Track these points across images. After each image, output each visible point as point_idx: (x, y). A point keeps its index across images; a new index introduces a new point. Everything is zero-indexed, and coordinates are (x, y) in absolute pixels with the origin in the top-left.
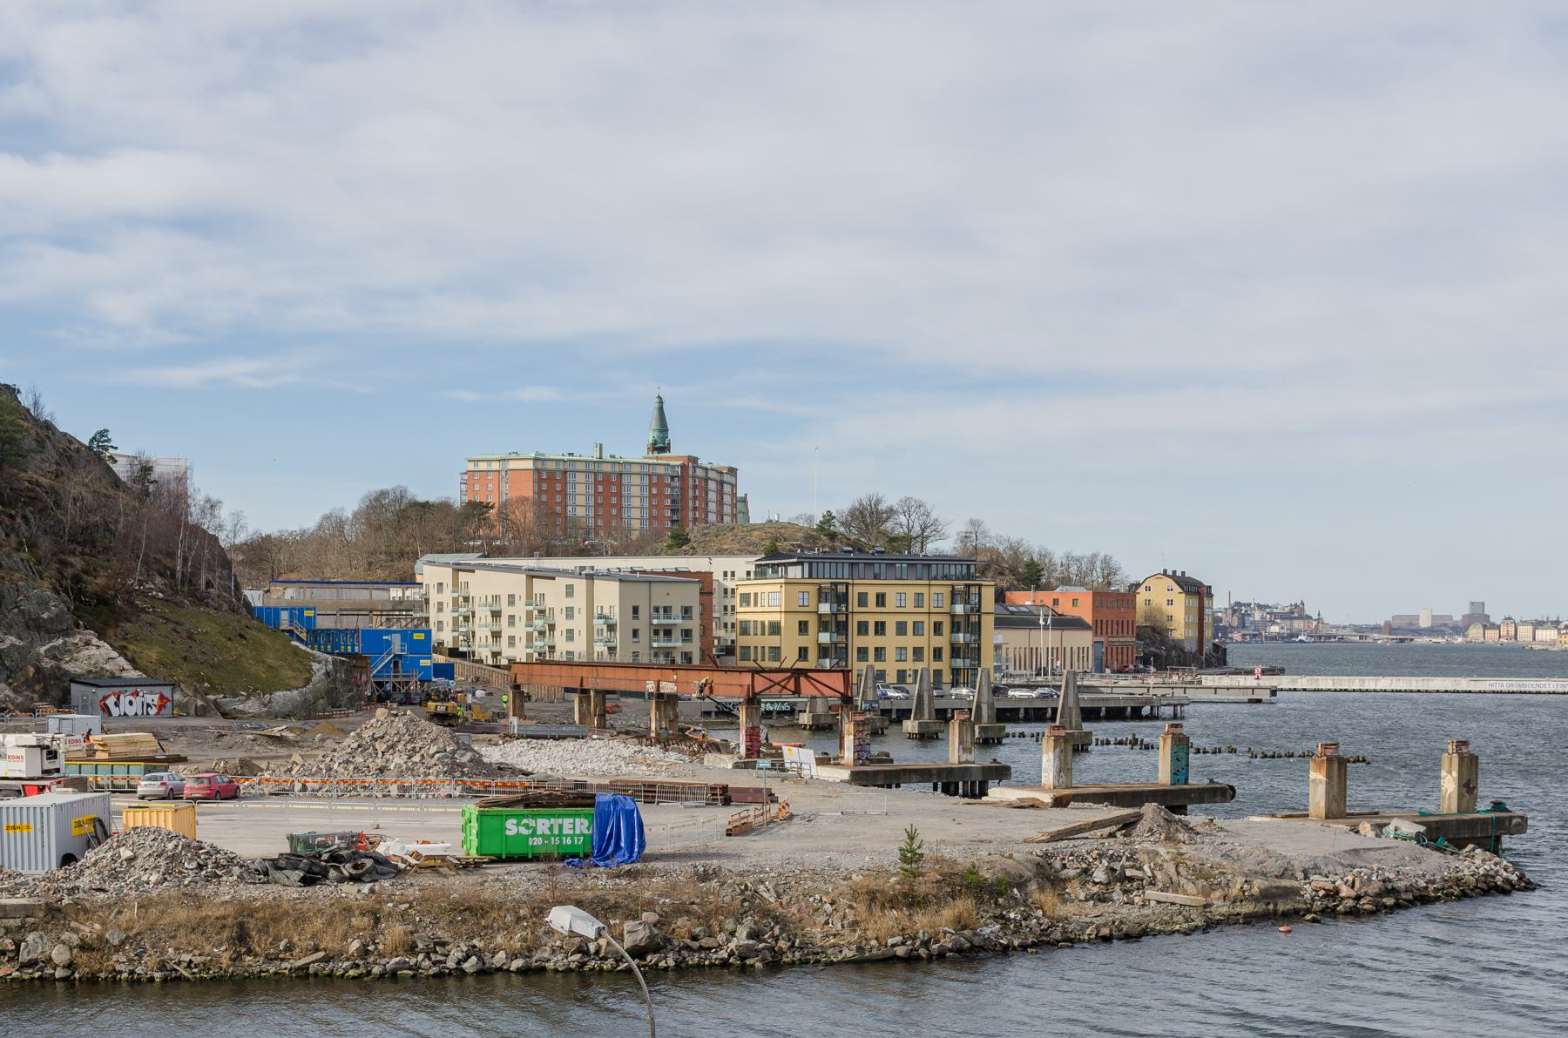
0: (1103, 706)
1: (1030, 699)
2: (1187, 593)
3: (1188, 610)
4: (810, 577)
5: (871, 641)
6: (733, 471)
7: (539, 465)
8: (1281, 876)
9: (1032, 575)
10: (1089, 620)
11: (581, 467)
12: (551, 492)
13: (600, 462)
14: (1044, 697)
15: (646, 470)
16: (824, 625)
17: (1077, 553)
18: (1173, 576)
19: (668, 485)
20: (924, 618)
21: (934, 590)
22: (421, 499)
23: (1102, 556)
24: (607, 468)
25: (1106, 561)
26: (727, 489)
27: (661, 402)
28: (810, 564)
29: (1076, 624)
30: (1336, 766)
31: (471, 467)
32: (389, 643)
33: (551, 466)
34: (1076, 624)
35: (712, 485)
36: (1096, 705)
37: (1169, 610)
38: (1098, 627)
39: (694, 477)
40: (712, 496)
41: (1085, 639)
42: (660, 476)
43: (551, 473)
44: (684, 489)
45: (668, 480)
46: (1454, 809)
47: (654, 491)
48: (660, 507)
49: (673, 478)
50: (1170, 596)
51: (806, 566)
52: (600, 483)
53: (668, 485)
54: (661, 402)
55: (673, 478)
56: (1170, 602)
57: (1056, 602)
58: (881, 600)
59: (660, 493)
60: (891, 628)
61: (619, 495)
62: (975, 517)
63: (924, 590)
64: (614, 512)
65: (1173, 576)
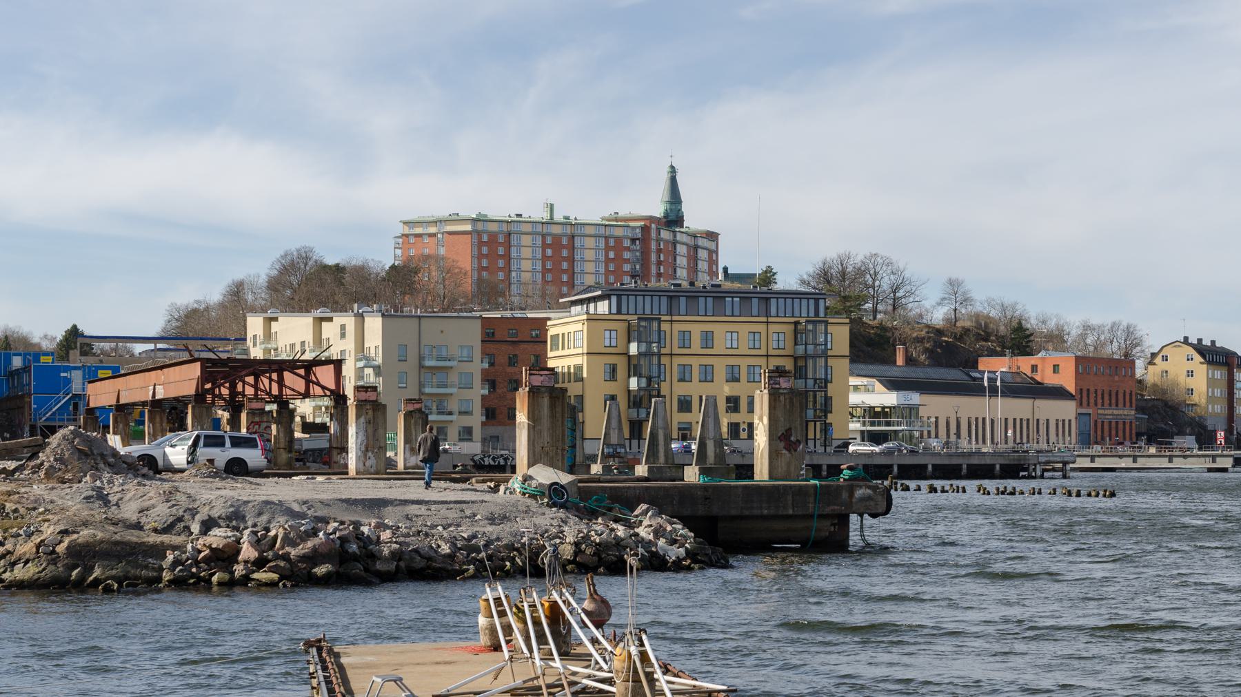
0: (964, 462)
1: (871, 455)
2: (1210, 363)
3: (1211, 382)
4: (619, 312)
5: (694, 389)
6: (712, 236)
7: (480, 226)
8: (167, 530)
9: (1020, 340)
10: (1071, 388)
11: (528, 228)
12: (492, 256)
13: (551, 222)
14: (889, 452)
15: (602, 231)
16: (634, 368)
17: (1095, 321)
18: (1200, 349)
19: (628, 249)
20: (762, 361)
21: (773, 328)
22: (330, 261)
23: (1125, 324)
24: (557, 230)
25: (1129, 331)
26: (703, 254)
27: (673, 170)
28: (619, 297)
29: (1058, 393)
30: (545, 401)
31: (407, 231)
32: (68, 381)
33: (493, 227)
34: (1058, 393)
35: (681, 249)
36: (955, 461)
37: (1191, 383)
38: (1081, 396)
39: (658, 240)
40: (682, 261)
41: (1067, 410)
42: (618, 240)
43: (493, 236)
44: (645, 253)
45: (627, 243)
46: (766, 477)
47: (612, 255)
48: (618, 273)
49: (633, 240)
50: (1190, 366)
51: (614, 299)
52: (549, 246)
53: (628, 249)
54: (673, 170)
55: (633, 240)
56: (1190, 373)
57: (1034, 368)
58: (707, 339)
59: (618, 257)
60: (720, 373)
61: (571, 260)
62: (954, 276)
63: (761, 328)
64: (501, 263)
65: (1200, 349)
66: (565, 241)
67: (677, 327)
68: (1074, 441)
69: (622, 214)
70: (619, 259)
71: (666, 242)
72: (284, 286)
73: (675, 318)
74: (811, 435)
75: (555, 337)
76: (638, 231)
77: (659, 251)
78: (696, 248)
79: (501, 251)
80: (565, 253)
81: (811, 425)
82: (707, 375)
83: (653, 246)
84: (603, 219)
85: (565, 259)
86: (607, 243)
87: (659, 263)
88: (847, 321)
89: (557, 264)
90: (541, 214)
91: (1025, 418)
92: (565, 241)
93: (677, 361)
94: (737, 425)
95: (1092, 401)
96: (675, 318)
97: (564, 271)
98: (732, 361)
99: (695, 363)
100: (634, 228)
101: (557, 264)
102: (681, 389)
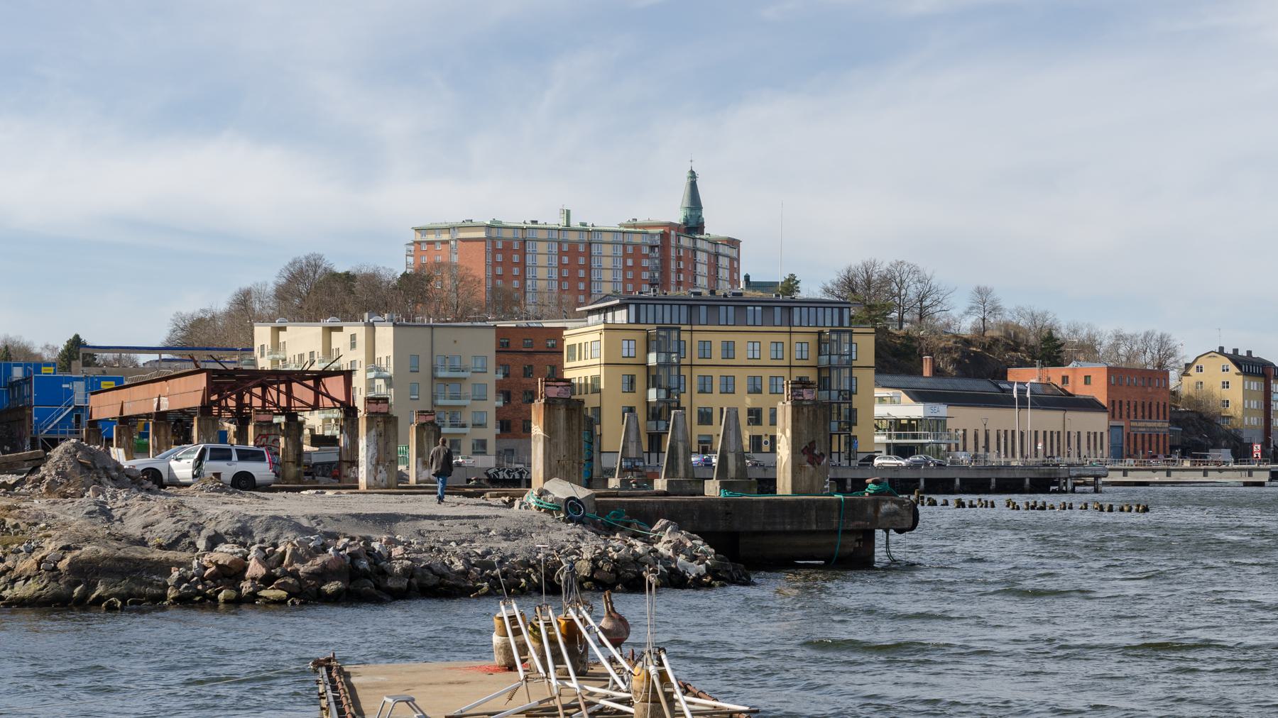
0: (993, 476)
1: (897, 468)
2: (1246, 374)
3: (1247, 394)
4: (638, 321)
5: (715, 401)
6: (734, 243)
7: (494, 233)
9: (1050, 350)
10: (1103, 400)
11: (544, 235)
12: (507, 264)
13: (568, 228)
14: (916, 466)
15: (620, 238)
16: (653, 379)
17: (1128, 331)
18: (1236, 359)
19: (647, 256)
20: (785, 372)
21: (796, 338)
22: (340, 268)
23: (1158, 334)
24: (573, 237)
25: (1163, 341)
26: (724, 262)
27: (693, 175)
28: (638, 306)
29: (1089, 405)
30: (562, 413)
31: (419, 238)
32: (70, 393)
33: (508, 234)
34: (1089, 405)
35: (702, 257)
36: (983, 475)
37: (1226, 394)
38: (1114, 408)
39: (678, 247)
40: (702, 269)
41: (1098, 422)
42: (637, 247)
43: (508, 243)
44: (665, 261)
45: (646, 250)
46: (789, 491)
47: (630, 262)
48: (637, 281)
49: (652, 248)
50: (1225, 377)
51: (632, 308)
52: (566, 253)
53: (647, 256)
54: (693, 175)
55: (652, 248)
56: (1226, 385)
57: (1065, 379)
58: (729, 349)
59: (637, 265)
60: (742, 384)
61: (588, 268)
62: (982, 285)
63: (784, 338)
64: (516, 271)
65: (1236, 359)
66: (581, 248)
67: (698, 337)
68: (1106, 454)
69: (640, 220)
70: (637, 267)
71: (686, 249)
72: (292, 295)
73: (695, 328)
74: (835, 448)
75: (572, 347)
76: (657, 238)
77: (679, 259)
78: (717, 255)
79: (516, 258)
80: (582, 261)
81: (835, 438)
82: (728, 387)
83: (673, 253)
84: (621, 225)
85: (582, 267)
86: (625, 250)
87: (679, 271)
88: (873, 330)
89: (573, 272)
90: (557, 221)
91: (1055, 430)
92: (581, 248)
93: (698, 372)
94: (759, 438)
95: (1125, 413)
96: (695, 328)
97: (581, 279)
98: (754, 372)
99: (716, 373)
100: (653, 235)
101: (573, 272)
102: (701, 401)
